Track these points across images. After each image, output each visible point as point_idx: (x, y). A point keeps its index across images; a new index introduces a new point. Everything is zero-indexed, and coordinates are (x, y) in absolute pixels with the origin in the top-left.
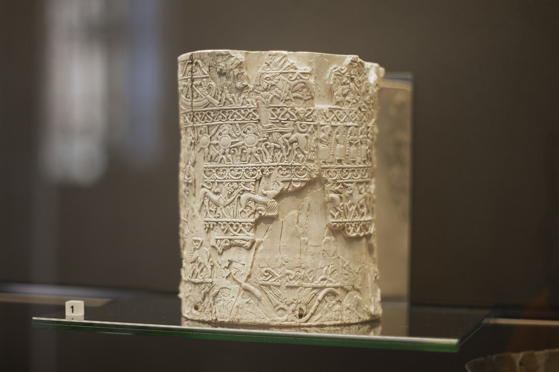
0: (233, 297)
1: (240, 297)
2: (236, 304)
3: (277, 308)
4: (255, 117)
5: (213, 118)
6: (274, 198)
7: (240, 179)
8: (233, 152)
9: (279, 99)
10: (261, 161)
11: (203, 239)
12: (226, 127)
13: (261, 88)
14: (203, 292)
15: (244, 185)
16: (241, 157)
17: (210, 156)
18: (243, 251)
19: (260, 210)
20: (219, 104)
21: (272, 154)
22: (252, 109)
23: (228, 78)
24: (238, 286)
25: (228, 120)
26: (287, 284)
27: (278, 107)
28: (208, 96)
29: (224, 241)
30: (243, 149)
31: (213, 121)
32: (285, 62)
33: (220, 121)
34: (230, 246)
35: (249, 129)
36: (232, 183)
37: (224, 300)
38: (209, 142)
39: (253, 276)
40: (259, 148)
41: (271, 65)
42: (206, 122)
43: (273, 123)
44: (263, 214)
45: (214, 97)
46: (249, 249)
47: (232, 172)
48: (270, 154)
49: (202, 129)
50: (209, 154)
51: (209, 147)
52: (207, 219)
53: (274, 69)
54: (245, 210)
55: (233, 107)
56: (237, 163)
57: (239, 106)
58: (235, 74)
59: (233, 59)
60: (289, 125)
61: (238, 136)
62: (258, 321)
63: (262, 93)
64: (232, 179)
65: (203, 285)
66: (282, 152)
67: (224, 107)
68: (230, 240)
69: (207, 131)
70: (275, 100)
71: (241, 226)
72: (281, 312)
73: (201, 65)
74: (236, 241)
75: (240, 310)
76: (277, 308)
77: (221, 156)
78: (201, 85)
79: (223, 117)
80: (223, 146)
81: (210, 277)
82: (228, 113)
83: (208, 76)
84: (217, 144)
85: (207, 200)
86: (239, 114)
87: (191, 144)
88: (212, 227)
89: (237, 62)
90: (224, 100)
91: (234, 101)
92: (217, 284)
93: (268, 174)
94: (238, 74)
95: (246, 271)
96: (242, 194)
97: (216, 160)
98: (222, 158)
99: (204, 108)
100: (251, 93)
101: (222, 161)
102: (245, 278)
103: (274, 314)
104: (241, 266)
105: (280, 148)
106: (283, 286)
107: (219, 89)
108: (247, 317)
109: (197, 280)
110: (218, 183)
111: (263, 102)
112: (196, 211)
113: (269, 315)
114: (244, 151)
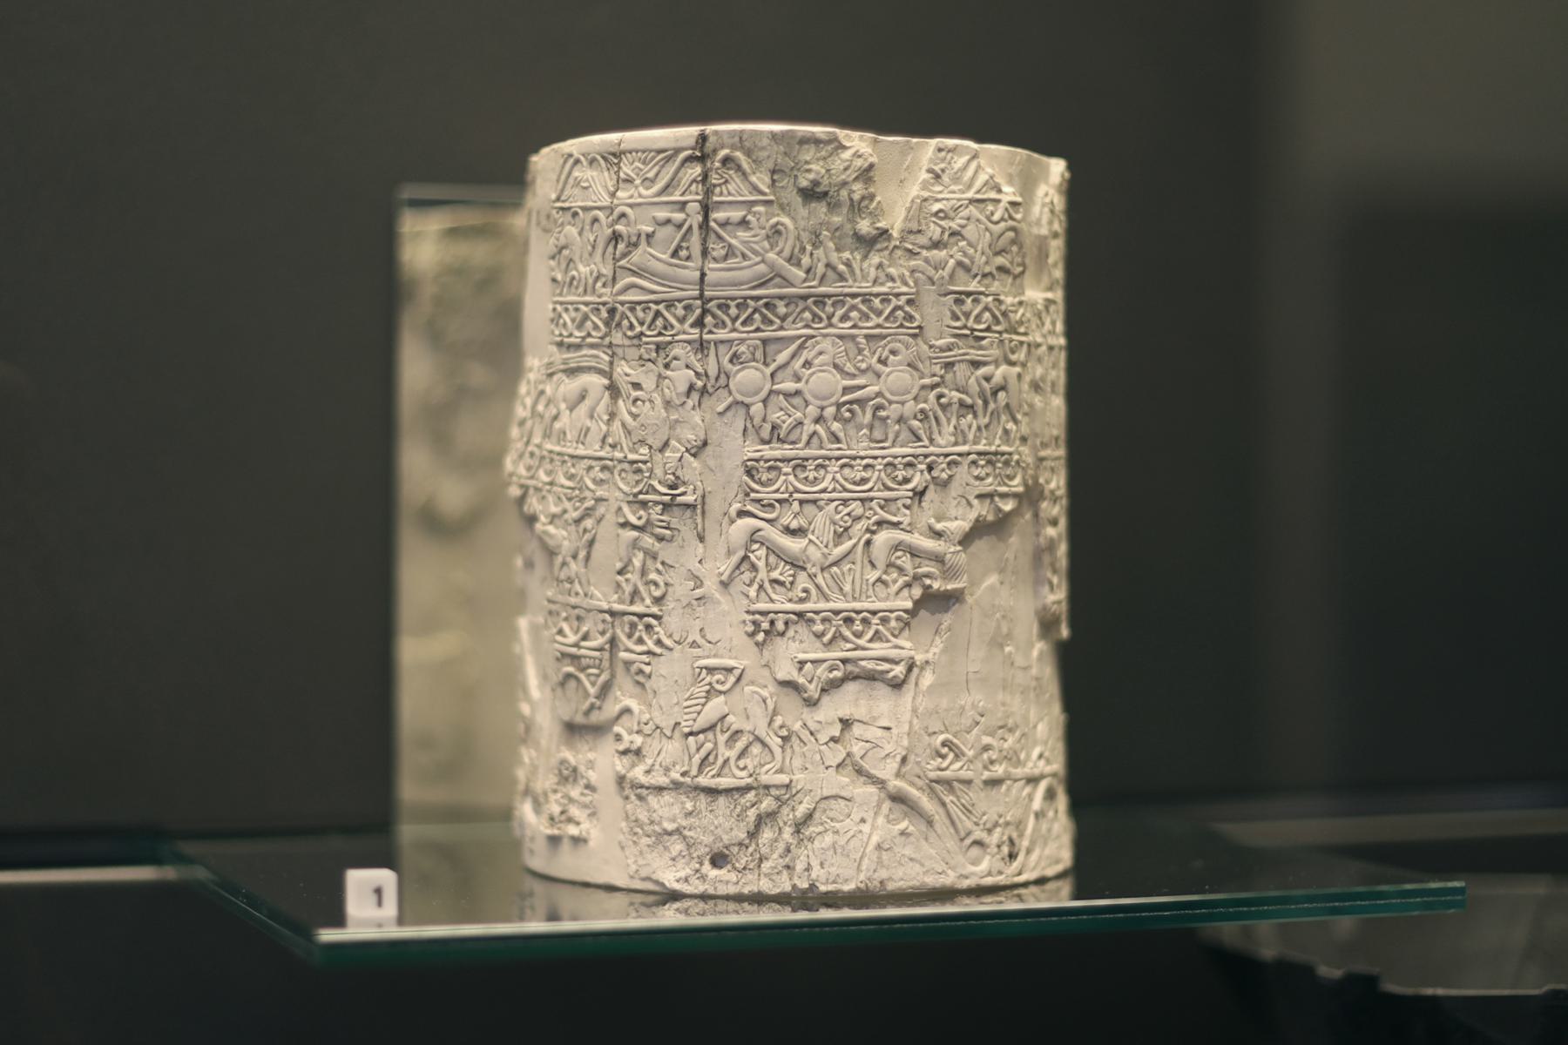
0: (863, 821)
1: (881, 820)
2: (875, 839)
3: (968, 841)
4: (910, 318)
5: (783, 319)
6: (960, 543)
7: (870, 490)
8: (847, 415)
9: (967, 269)
10: (926, 442)
11: (745, 662)
12: (826, 344)
13: (922, 240)
14: (752, 814)
15: (882, 508)
16: (871, 427)
17: (768, 427)
18: (882, 690)
19: (927, 576)
20: (805, 281)
21: (954, 421)
22: (903, 298)
23: (834, 207)
24: (872, 789)
25: (831, 325)
26: (986, 775)
27: (969, 294)
28: (771, 256)
29: (825, 665)
30: (879, 407)
31: (781, 328)
32: (976, 172)
33: (807, 326)
34: (848, 678)
35: (893, 352)
36: (845, 502)
37: (837, 832)
38: (768, 387)
39: (912, 758)
40: (922, 405)
41: (945, 178)
42: (758, 330)
43: (956, 336)
44: (936, 585)
45: (789, 260)
46: (897, 685)
47: (847, 471)
48: (949, 420)
49: (743, 348)
50: (764, 420)
51: (765, 401)
52: (761, 606)
53: (953, 188)
54: (885, 577)
55: (847, 290)
56: (861, 447)
57: (865, 287)
58: (856, 197)
59: (847, 155)
60: (992, 344)
61: (863, 372)
62: (932, 881)
63: (925, 253)
64: (846, 490)
65: (751, 796)
66: (975, 416)
67: (822, 289)
68: (844, 661)
69: (759, 354)
70: (961, 273)
71: (875, 620)
72: (975, 851)
73: (745, 166)
74: (863, 663)
75: (885, 856)
76: (968, 841)
77: (809, 427)
78: (743, 223)
79: (815, 315)
80: (816, 397)
81: (781, 771)
82: (833, 305)
83: (772, 198)
84: (798, 393)
85: (762, 552)
86: (864, 308)
87: (691, 388)
88: (780, 626)
89: (859, 163)
90: (820, 269)
91: (852, 272)
92: (808, 787)
93: (944, 476)
94: (863, 198)
95: (894, 746)
96: (873, 532)
97: (792, 437)
98: (815, 433)
99: (754, 288)
100: (899, 252)
101: (815, 440)
102: (893, 765)
103: (960, 858)
104: (880, 733)
105: (972, 407)
106: (978, 782)
107: (805, 236)
108: (905, 876)
109: (725, 782)
110: (801, 502)
111: (930, 279)
112: (710, 586)
113: (952, 863)
114: (883, 413)
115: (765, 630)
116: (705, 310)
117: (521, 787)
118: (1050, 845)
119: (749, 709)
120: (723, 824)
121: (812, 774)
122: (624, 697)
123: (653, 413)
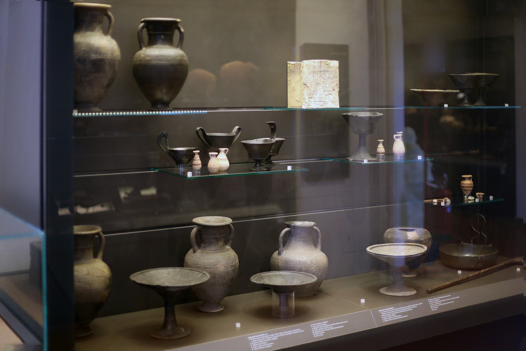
115: (324, 91)
116: (320, 71)
117: (443, 250)
118: (338, 107)
119: (323, 96)
120: (321, 103)
121: (327, 100)
122: (314, 96)
123: (317, 78)
